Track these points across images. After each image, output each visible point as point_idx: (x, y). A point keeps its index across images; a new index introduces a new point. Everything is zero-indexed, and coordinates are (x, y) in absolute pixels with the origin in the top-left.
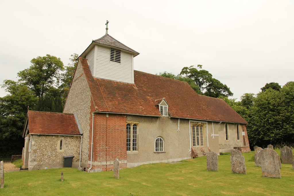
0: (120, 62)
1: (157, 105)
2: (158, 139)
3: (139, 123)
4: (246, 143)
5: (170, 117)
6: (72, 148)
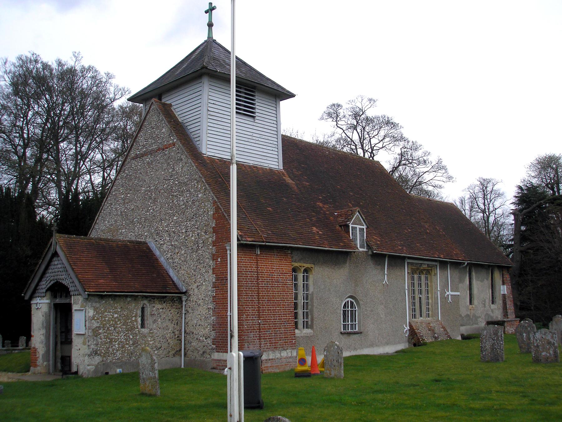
0: (254, 117)
1: (344, 223)
2: (348, 301)
3: (313, 266)
4: (509, 311)
5: (370, 253)
6: (165, 325)
